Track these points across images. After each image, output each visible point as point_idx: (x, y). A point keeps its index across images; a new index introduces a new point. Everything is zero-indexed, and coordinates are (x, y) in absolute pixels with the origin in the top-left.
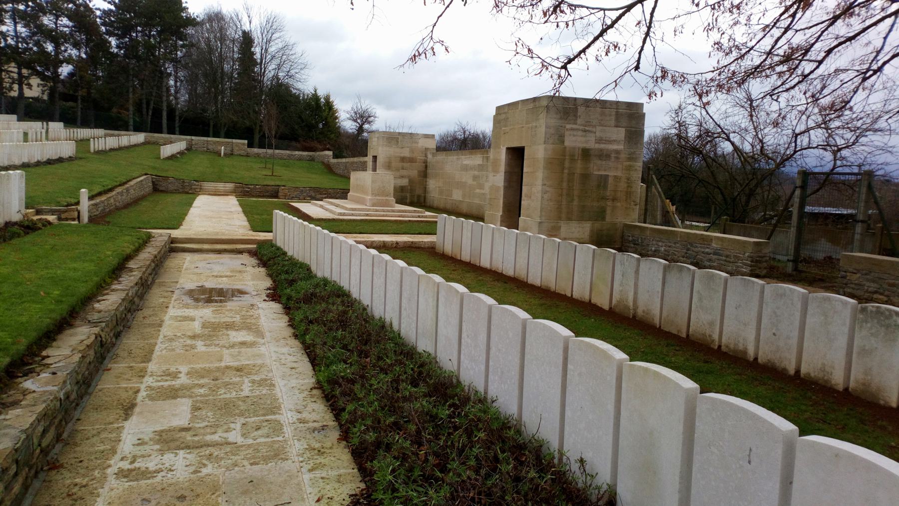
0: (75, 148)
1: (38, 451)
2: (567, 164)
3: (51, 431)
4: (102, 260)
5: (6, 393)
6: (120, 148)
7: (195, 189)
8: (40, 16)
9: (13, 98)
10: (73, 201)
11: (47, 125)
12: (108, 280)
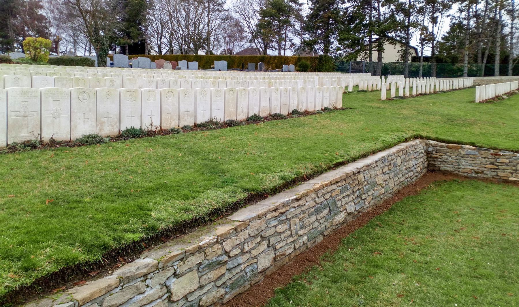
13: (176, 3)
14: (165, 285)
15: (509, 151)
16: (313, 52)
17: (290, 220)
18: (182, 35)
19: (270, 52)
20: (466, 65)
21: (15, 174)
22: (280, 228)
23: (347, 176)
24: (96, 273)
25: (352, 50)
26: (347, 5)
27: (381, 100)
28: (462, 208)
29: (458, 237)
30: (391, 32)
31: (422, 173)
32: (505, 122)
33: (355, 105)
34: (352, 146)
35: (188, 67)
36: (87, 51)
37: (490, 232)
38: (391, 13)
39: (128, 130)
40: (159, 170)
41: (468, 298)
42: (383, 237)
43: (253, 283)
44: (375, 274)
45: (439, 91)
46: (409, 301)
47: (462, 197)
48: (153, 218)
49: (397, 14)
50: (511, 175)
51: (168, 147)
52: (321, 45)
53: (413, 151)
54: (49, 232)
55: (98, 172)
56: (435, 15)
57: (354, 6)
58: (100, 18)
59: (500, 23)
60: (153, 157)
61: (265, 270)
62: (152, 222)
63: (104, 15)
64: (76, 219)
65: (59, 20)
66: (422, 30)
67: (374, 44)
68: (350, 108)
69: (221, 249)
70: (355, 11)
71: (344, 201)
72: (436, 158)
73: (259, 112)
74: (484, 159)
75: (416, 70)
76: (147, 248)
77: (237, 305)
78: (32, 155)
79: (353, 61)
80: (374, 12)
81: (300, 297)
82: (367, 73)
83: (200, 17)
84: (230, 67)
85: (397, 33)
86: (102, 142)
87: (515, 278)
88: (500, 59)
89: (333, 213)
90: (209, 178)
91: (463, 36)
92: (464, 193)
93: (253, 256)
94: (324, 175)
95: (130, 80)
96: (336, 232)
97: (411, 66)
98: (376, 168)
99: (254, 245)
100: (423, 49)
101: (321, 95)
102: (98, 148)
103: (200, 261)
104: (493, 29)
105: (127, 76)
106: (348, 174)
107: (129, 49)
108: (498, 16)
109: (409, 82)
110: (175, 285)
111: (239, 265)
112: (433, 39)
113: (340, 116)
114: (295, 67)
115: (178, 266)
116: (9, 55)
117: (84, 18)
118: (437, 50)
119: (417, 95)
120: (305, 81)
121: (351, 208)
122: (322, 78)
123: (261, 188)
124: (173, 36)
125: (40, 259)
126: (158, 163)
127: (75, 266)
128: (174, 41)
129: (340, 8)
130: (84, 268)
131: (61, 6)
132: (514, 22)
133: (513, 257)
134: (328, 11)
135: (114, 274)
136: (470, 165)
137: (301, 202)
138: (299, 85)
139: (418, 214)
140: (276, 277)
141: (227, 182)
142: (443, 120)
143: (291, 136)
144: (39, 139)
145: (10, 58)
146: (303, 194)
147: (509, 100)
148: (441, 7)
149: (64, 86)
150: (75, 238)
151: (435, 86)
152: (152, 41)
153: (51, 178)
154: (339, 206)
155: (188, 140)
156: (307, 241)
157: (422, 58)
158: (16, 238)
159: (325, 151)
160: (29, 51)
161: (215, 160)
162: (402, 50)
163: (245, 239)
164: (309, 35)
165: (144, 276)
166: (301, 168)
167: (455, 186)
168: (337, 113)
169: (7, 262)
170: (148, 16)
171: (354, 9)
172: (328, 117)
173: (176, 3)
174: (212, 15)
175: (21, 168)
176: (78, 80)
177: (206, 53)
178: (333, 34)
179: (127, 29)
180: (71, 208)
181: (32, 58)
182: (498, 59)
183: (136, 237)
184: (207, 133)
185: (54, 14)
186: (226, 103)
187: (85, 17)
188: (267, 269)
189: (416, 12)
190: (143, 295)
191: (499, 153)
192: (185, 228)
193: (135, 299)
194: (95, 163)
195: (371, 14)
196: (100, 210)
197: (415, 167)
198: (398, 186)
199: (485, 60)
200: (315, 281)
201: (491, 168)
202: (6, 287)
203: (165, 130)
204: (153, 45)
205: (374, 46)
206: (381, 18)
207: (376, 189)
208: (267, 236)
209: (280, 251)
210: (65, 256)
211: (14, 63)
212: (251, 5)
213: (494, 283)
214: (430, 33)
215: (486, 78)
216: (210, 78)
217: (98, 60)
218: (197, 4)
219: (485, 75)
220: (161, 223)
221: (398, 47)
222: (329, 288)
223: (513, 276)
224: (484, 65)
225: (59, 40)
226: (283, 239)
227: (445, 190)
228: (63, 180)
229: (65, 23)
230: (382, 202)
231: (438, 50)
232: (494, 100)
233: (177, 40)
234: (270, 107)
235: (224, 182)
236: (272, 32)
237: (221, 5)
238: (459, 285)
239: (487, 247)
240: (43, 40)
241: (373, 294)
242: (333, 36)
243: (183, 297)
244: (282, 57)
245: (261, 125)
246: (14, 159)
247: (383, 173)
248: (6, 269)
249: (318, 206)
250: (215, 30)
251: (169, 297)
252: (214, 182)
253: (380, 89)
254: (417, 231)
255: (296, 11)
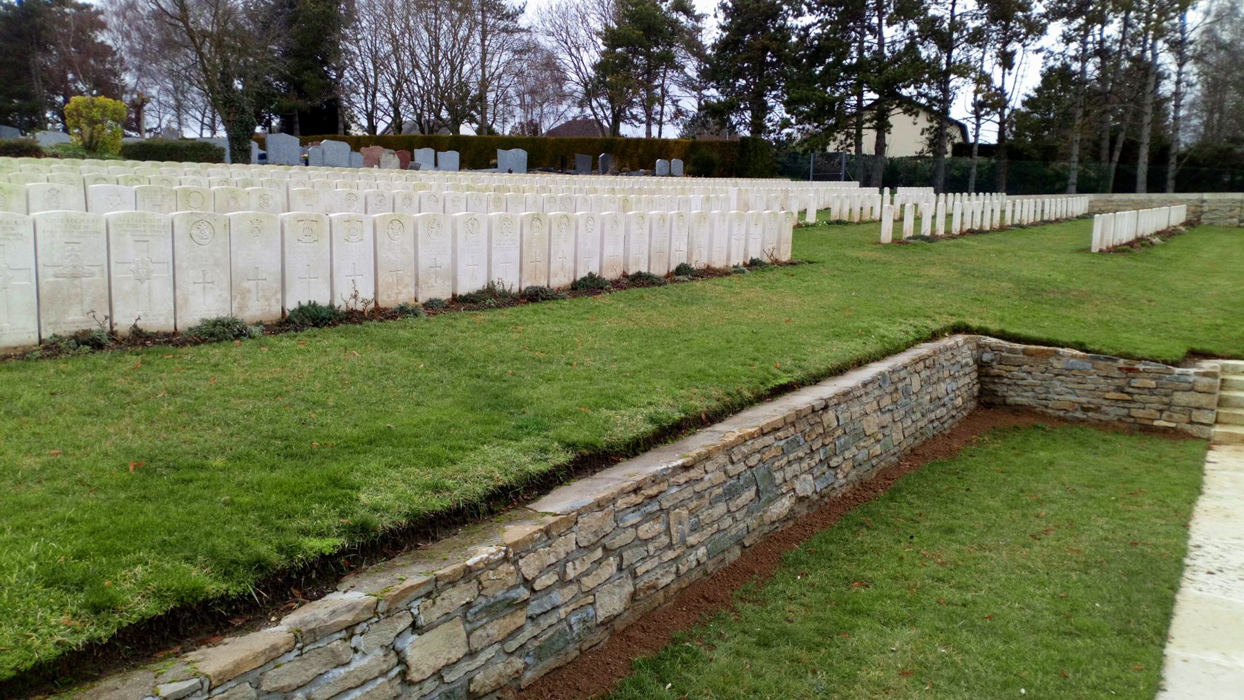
7: (1188, 409)
13: (409, 13)
14: (393, 649)
15: (1158, 362)
16: (726, 131)
17: (668, 513)
18: (423, 89)
19: (626, 130)
20: (1075, 165)
21: (60, 404)
22: (646, 530)
23: (799, 416)
24: (243, 621)
25: (817, 127)
26: (807, 19)
27: (879, 243)
28: (1049, 486)
29: (1037, 548)
30: (908, 86)
31: (965, 409)
32: (1154, 297)
33: (820, 256)
34: (810, 349)
35: (436, 164)
36: (205, 127)
37: (1106, 539)
38: (908, 41)
39: (302, 309)
40: (374, 400)
41: (1049, 677)
42: (874, 550)
43: (586, 646)
44: (852, 628)
45: (1013, 225)
46: (923, 684)
47: (1051, 463)
48: (364, 506)
49: (922, 44)
50: (1158, 415)
51: (394, 348)
52: (746, 114)
53: (948, 361)
54: (138, 531)
55: (239, 402)
56: (1009, 48)
57: (823, 24)
58: (234, 49)
59: (1152, 70)
60: (360, 371)
61: (612, 620)
62: (361, 514)
63: (243, 43)
64: (195, 506)
65: (141, 54)
66: (977, 81)
67: (867, 112)
68: (810, 263)
69: (515, 574)
70: (825, 34)
71: (789, 473)
72: (999, 376)
73: (601, 268)
74: (1102, 380)
75: (963, 175)
76: (351, 569)
77: (550, 691)
78: (94, 364)
79: (818, 152)
80: (869, 37)
81: (689, 675)
82: (850, 180)
83: (464, 47)
84: (534, 165)
85: (920, 87)
86: (245, 335)
87: (1150, 634)
88: (1151, 155)
89: (764, 498)
90: (486, 418)
91: (1069, 99)
92: (1055, 455)
93: (584, 589)
94: (747, 414)
95: (303, 193)
96: (770, 538)
97: (950, 165)
98: (864, 398)
99: (587, 566)
100: (978, 126)
101: (743, 232)
102: (237, 349)
103: (468, 599)
104: (1137, 84)
105: (297, 184)
106: (800, 411)
107: (300, 122)
108: (1149, 54)
109: (946, 202)
110: (413, 648)
111: (555, 608)
112: (1002, 103)
113: (785, 279)
114: (685, 165)
115: (422, 609)
116: (34, 137)
117: (198, 50)
118: (1011, 131)
119: (962, 234)
120: (708, 199)
121: (806, 486)
122: (747, 191)
123: (603, 441)
124: (400, 92)
125: (124, 588)
126: (370, 383)
127: (199, 604)
128: (404, 103)
129: (792, 28)
130: (218, 609)
131: (145, 23)
132: (1185, 69)
133: (1150, 591)
134: (763, 33)
135: (282, 622)
136: (1073, 392)
137: (693, 474)
138: (693, 206)
139: (953, 501)
140: (637, 634)
141: (526, 427)
142: (1017, 291)
143: (673, 325)
144: (108, 328)
145: (39, 144)
146: (699, 455)
147: (1164, 247)
148: (1023, 30)
149: (158, 208)
150: (195, 547)
151: (1003, 212)
152: (352, 104)
153: (136, 415)
154: (778, 481)
155: (439, 333)
156: (705, 559)
157: (976, 148)
158: (70, 543)
159: (751, 359)
160: (78, 127)
161: (499, 378)
162: (932, 127)
163: (568, 554)
164: (717, 89)
165: (347, 629)
166: (694, 397)
167: (1036, 440)
168: (779, 273)
169: (55, 593)
170: (344, 45)
171: (823, 30)
172: (757, 282)
173: (409, 13)
174: (492, 42)
175: (71, 392)
176: (188, 193)
177: (479, 131)
178: (774, 88)
179: (296, 74)
180: (184, 481)
181: (84, 144)
182: (1144, 153)
183: (327, 545)
184: (483, 317)
185: (131, 42)
186: (524, 248)
187: (201, 48)
188: (616, 617)
189: (967, 41)
190: (347, 669)
191: (1136, 366)
192: (435, 528)
193: (330, 675)
194: (232, 383)
195: (862, 42)
196: (245, 485)
197: (952, 395)
198: (912, 440)
199: (1117, 155)
200: (721, 643)
201: (1117, 400)
202: (58, 643)
203: (386, 309)
204: (356, 112)
205: (868, 117)
206: (886, 51)
207: (862, 444)
208: (616, 546)
209: (646, 578)
210: (175, 583)
211: (46, 156)
212: (583, 18)
213: (1105, 645)
214: (997, 90)
215: (1117, 197)
216: (487, 189)
217: (232, 148)
218: (457, 15)
219: (1115, 190)
220: (382, 516)
221: (923, 121)
222: (751, 657)
223: (1146, 629)
224: (1114, 165)
225: (144, 101)
226: (652, 553)
227: (1014, 448)
228: (163, 418)
229: (156, 61)
230: (874, 474)
231: (1014, 129)
232: (1132, 247)
233: (411, 101)
234: (626, 258)
235: (521, 427)
236: (632, 82)
237: (512, 16)
238: (1031, 649)
239: (1096, 570)
240: (109, 102)
241: (848, 671)
242: (774, 93)
243: (434, 674)
244: (654, 140)
245: (603, 299)
246: (57, 372)
247: (880, 409)
248: (55, 607)
249: (732, 482)
250: (500, 77)
251: (403, 674)
252: (498, 428)
253: (878, 218)
254: (948, 537)
255: (687, 33)
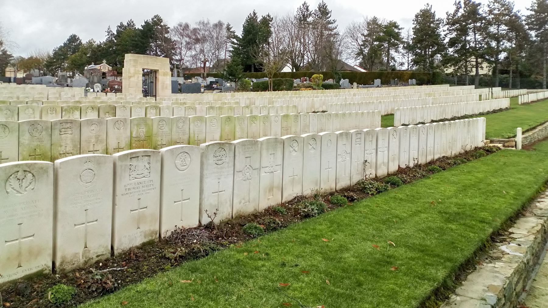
0: (509, 102)
1: (514, 293)
2: (277, 39)
3: (520, 282)
4: (537, 174)
5: (492, 251)
6: (538, 101)
8: (489, 27)
9: (472, 76)
10: (512, 135)
11: (492, 89)
12: (543, 188)
